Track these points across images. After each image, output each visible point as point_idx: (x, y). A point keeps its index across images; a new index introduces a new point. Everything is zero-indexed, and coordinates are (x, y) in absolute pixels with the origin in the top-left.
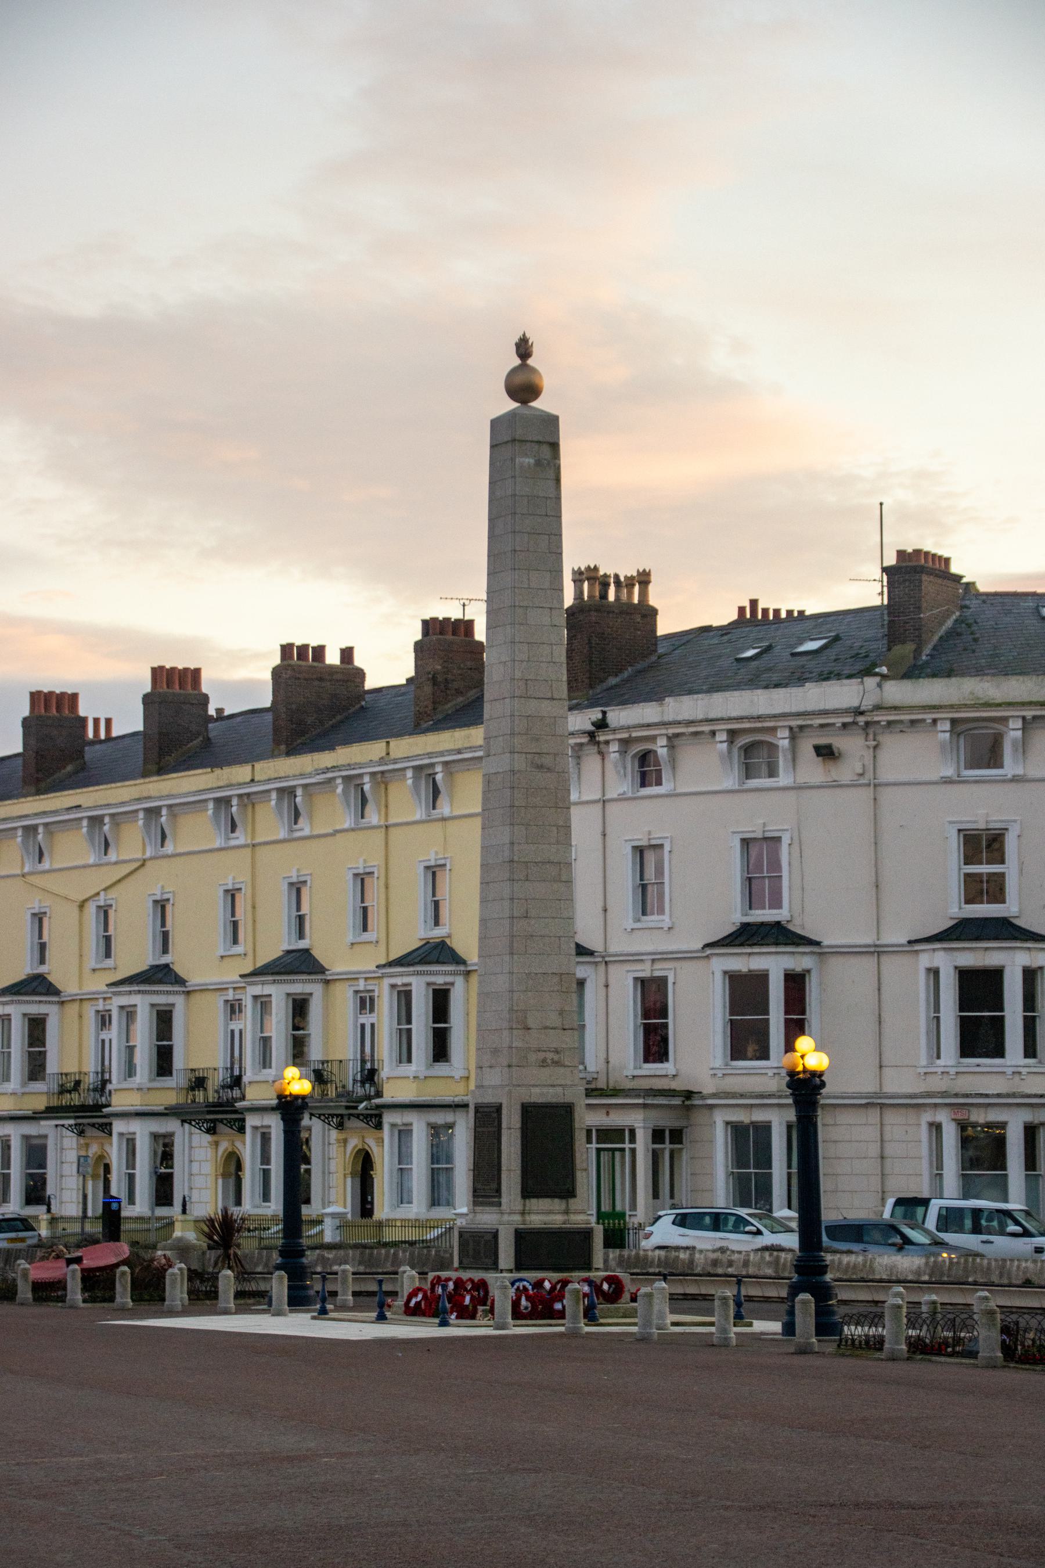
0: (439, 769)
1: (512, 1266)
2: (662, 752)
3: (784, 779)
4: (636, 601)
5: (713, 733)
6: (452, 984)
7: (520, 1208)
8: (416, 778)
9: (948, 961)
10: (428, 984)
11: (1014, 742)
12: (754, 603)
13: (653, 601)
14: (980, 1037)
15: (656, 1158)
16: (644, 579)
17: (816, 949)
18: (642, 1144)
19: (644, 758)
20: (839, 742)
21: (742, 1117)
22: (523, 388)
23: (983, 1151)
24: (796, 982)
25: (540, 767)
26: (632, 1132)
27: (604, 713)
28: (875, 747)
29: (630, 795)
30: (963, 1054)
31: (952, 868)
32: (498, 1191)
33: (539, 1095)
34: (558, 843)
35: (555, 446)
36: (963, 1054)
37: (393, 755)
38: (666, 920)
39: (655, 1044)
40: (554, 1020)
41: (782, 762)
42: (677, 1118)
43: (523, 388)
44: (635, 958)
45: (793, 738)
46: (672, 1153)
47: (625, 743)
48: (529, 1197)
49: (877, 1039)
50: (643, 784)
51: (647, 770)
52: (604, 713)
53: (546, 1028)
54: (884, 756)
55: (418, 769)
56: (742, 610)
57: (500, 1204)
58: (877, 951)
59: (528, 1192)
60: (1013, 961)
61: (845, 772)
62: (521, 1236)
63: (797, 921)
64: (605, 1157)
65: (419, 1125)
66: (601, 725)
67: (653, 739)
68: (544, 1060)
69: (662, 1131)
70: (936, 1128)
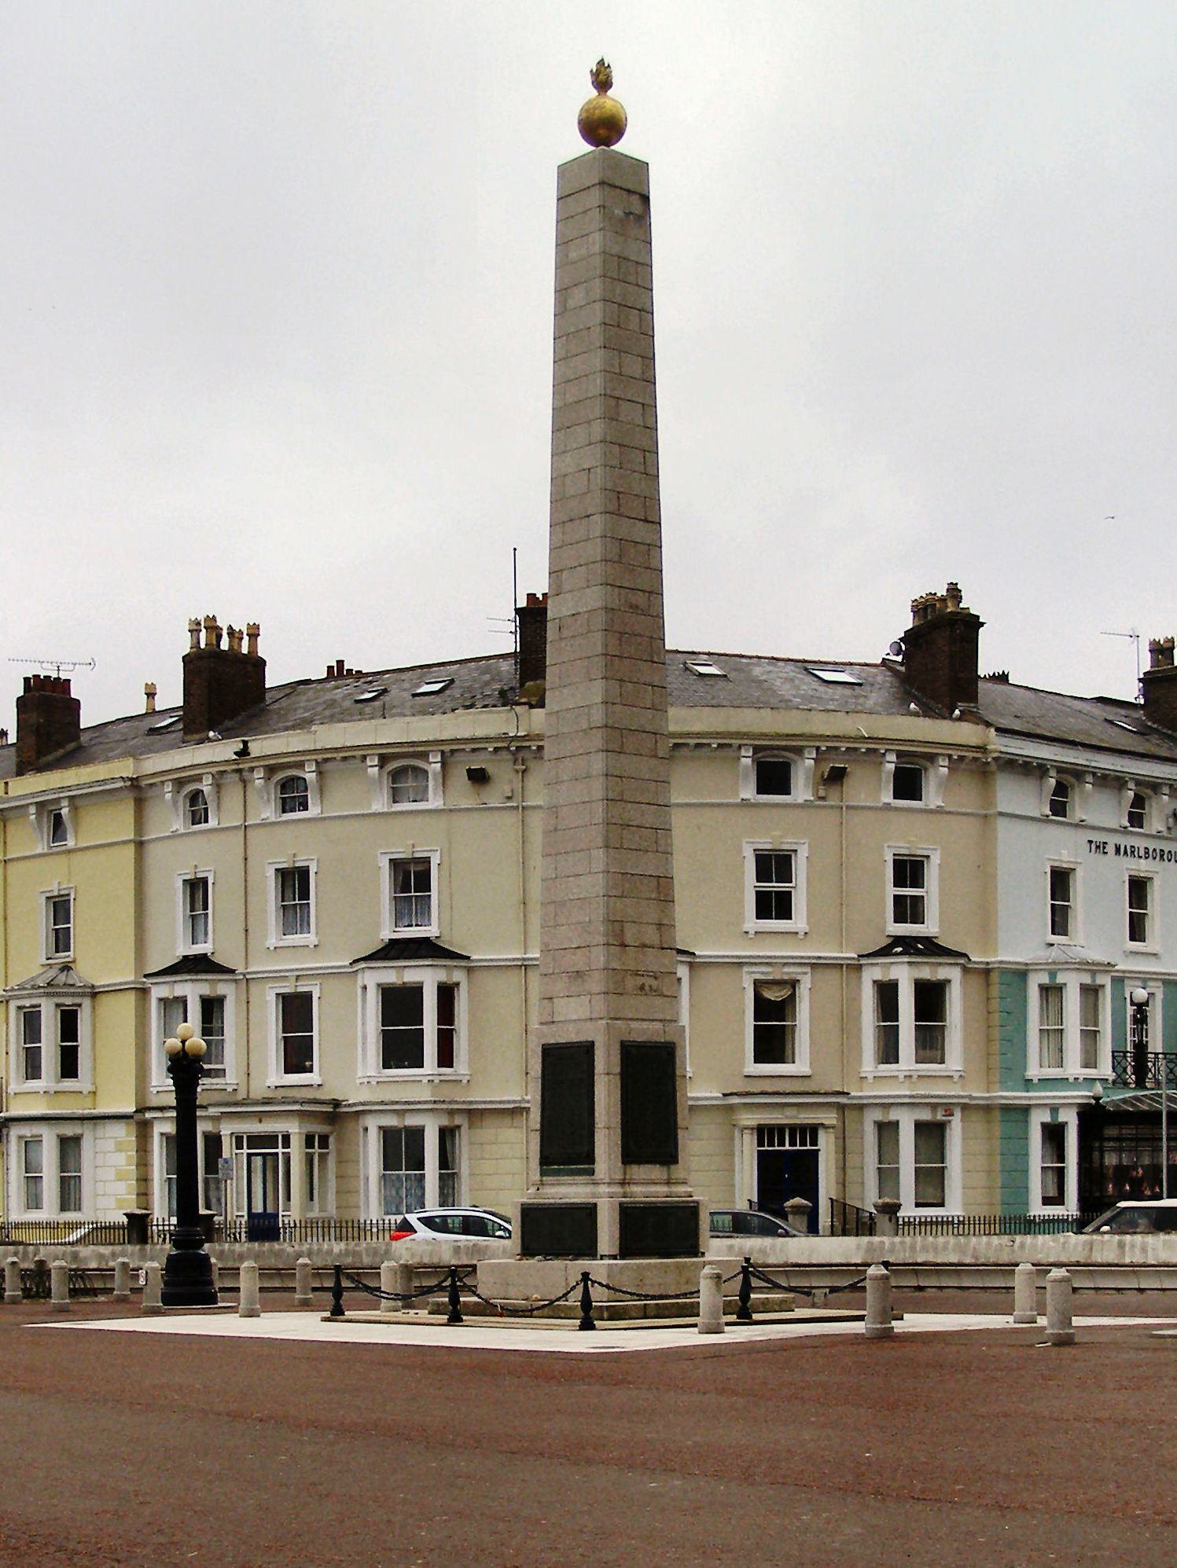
0: (65, 803)
1: (615, 1251)
2: (310, 777)
4: (245, 651)
6: (80, 1005)
7: (619, 1176)
8: (39, 814)
10: (58, 1005)
12: (340, 663)
13: (261, 653)
17: (463, 963)
18: (296, 1150)
19: (286, 785)
20: (491, 769)
21: (391, 1121)
22: (601, 128)
24: (446, 994)
26: (287, 1139)
27: (245, 743)
28: (524, 771)
29: (273, 819)
34: (653, 708)
35: (646, 199)
37: (11, 794)
38: (310, 938)
39: (297, 1056)
42: (332, 1120)
43: (601, 128)
44: (279, 977)
46: (320, 1155)
47: (271, 770)
48: (631, 1163)
50: (284, 811)
51: (292, 796)
52: (245, 743)
53: (645, 946)
55: (40, 805)
56: (330, 668)
57: (592, 1172)
61: (494, 796)
64: (258, 1162)
66: (244, 753)
67: (300, 765)
68: (642, 988)
69: (313, 1137)
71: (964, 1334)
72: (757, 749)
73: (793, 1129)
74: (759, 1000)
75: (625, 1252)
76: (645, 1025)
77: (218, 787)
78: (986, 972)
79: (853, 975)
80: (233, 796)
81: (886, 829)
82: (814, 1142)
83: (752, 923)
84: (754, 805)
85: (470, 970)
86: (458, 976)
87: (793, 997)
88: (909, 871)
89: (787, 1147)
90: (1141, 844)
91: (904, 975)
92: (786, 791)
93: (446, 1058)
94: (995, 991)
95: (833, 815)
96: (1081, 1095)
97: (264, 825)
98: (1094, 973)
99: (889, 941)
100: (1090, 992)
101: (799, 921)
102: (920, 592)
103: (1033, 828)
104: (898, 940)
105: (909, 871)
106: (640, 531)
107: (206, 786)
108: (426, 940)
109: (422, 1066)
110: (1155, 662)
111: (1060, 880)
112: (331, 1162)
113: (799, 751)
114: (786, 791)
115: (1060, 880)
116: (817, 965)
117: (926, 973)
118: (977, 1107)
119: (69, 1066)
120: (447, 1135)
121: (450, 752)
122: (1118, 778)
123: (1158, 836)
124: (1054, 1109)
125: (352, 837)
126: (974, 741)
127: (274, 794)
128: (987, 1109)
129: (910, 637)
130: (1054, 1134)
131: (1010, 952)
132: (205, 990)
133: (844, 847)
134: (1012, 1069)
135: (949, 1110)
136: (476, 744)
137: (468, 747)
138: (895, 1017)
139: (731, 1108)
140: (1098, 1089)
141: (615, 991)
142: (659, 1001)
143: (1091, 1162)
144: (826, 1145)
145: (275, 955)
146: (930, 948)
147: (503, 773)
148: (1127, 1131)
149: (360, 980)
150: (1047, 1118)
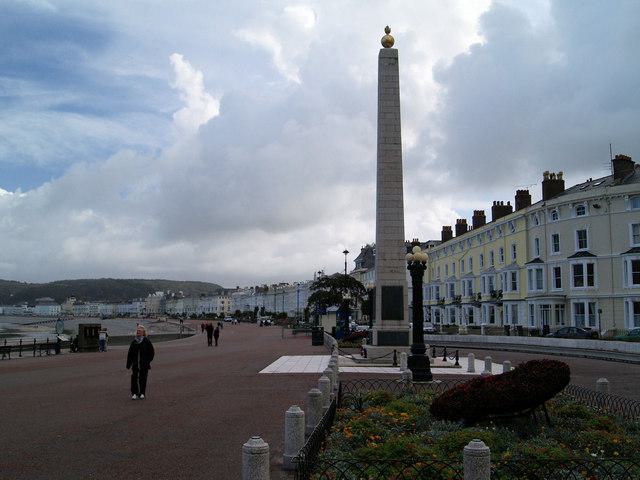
3: (587, 214)
9: (630, 258)
15: (557, 312)
16: (560, 174)
20: (600, 204)
22: (387, 43)
24: (590, 267)
30: (634, 283)
33: (388, 283)
35: (397, 59)
36: (634, 283)
40: (395, 256)
41: (586, 210)
47: (549, 210)
49: (614, 284)
61: (601, 211)
62: (380, 334)
65: (509, 304)
70: (627, 303)
71: (358, 374)
75: (379, 345)
86: (593, 261)
104: (634, 248)
106: (395, 147)
119: (514, 288)
127: (575, 212)
132: (589, 262)
138: (589, 277)
145: (553, 259)
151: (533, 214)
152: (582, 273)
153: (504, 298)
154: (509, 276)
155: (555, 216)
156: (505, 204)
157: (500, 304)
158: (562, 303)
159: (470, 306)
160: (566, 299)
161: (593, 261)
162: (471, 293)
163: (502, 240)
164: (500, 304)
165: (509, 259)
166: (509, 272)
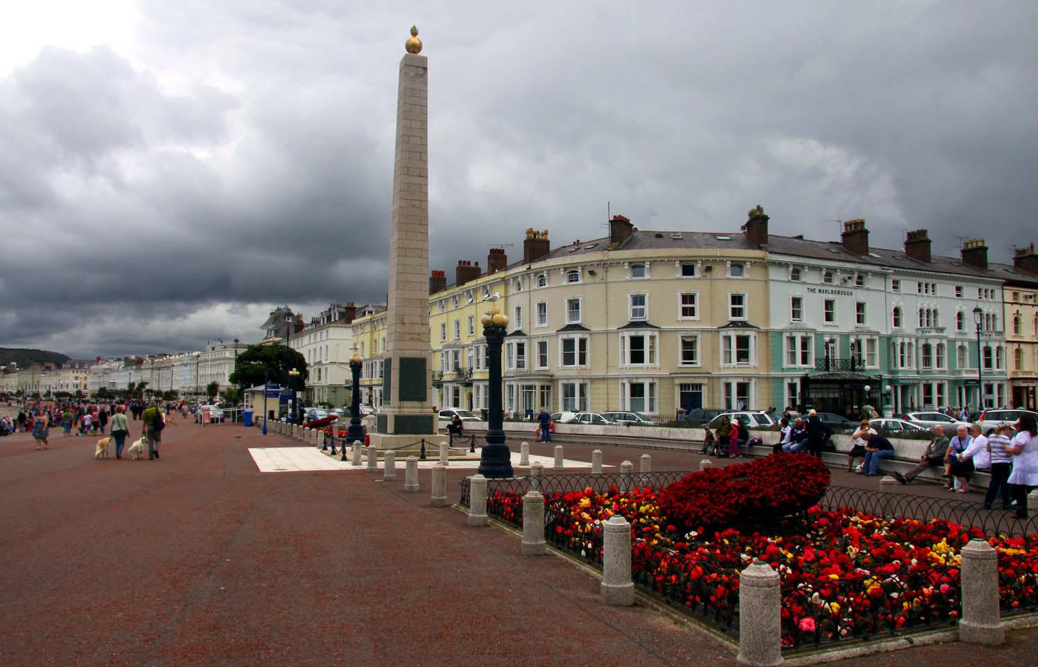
1: (393, 431)
3: (580, 281)
5: (559, 269)
9: (628, 334)
11: (647, 269)
12: (578, 241)
14: (637, 357)
15: (542, 394)
18: (538, 391)
20: (596, 270)
21: (565, 382)
22: (413, 48)
23: (637, 390)
24: (583, 343)
25: (414, 206)
30: (632, 362)
31: (630, 307)
32: (390, 398)
35: (425, 69)
38: (545, 325)
39: (543, 361)
44: (538, 337)
45: (582, 269)
47: (536, 273)
54: (609, 274)
57: (390, 403)
58: (607, 333)
59: (402, 398)
60: (646, 334)
61: (597, 279)
62: (398, 419)
63: (584, 323)
67: (542, 272)
68: (412, 338)
70: (624, 384)
72: (681, 261)
73: (693, 385)
74: (683, 342)
75: (396, 432)
76: (414, 351)
77: (523, 279)
78: (767, 332)
79: (716, 334)
80: (527, 281)
81: (726, 284)
82: (700, 389)
83: (680, 317)
84: (682, 279)
85: (591, 334)
86: (586, 336)
87: (696, 341)
88: (737, 299)
89: (691, 391)
90: (830, 289)
91: (733, 334)
92: (693, 274)
93: (582, 361)
94: (770, 339)
95: (708, 282)
96: (802, 373)
97: (535, 290)
98: (872, 335)
99: (729, 323)
100: (871, 342)
101: (697, 317)
102: (750, 209)
103: (785, 284)
105: (737, 299)
106: (418, 180)
107: (520, 279)
108: (578, 325)
109: (643, 362)
110: (846, 229)
111: (796, 302)
112: (551, 394)
113: (696, 261)
114: (693, 274)
115: (796, 302)
116: (703, 331)
117: (740, 333)
118: (764, 378)
120: (582, 387)
121: (584, 266)
122: (851, 271)
123: (837, 286)
124: (792, 378)
125: (558, 292)
126: (761, 256)
128: (767, 378)
129: (748, 225)
130: (792, 387)
131: (776, 325)
132: (518, 341)
133: (713, 294)
134: (778, 364)
135: (750, 378)
136: (591, 264)
137: (589, 264)
138: (580, 354)
139: (673, 378)
140: (807, 371)
141: (889, 341)
142: (422, 343)
143: (805, 395)
144: (704, 390)
146: (745, 325)
147: (600, 272)
148: (818, 386)
149: (621, 335)
150: (789, 381)
151: (483, 287)
152: (574, 350)
153: (475, 377)
154: (451, 355)
155: (542, 283)
156: (473, 265)
157: (469, 385)
158: (548, 384)
159: (455, 385)
160: (552, 379)
161: (586, 336)
162: (457, 368)
163: (473, 307)
164: (469, 385)
165: (451, 338)
166: (451, 351)
